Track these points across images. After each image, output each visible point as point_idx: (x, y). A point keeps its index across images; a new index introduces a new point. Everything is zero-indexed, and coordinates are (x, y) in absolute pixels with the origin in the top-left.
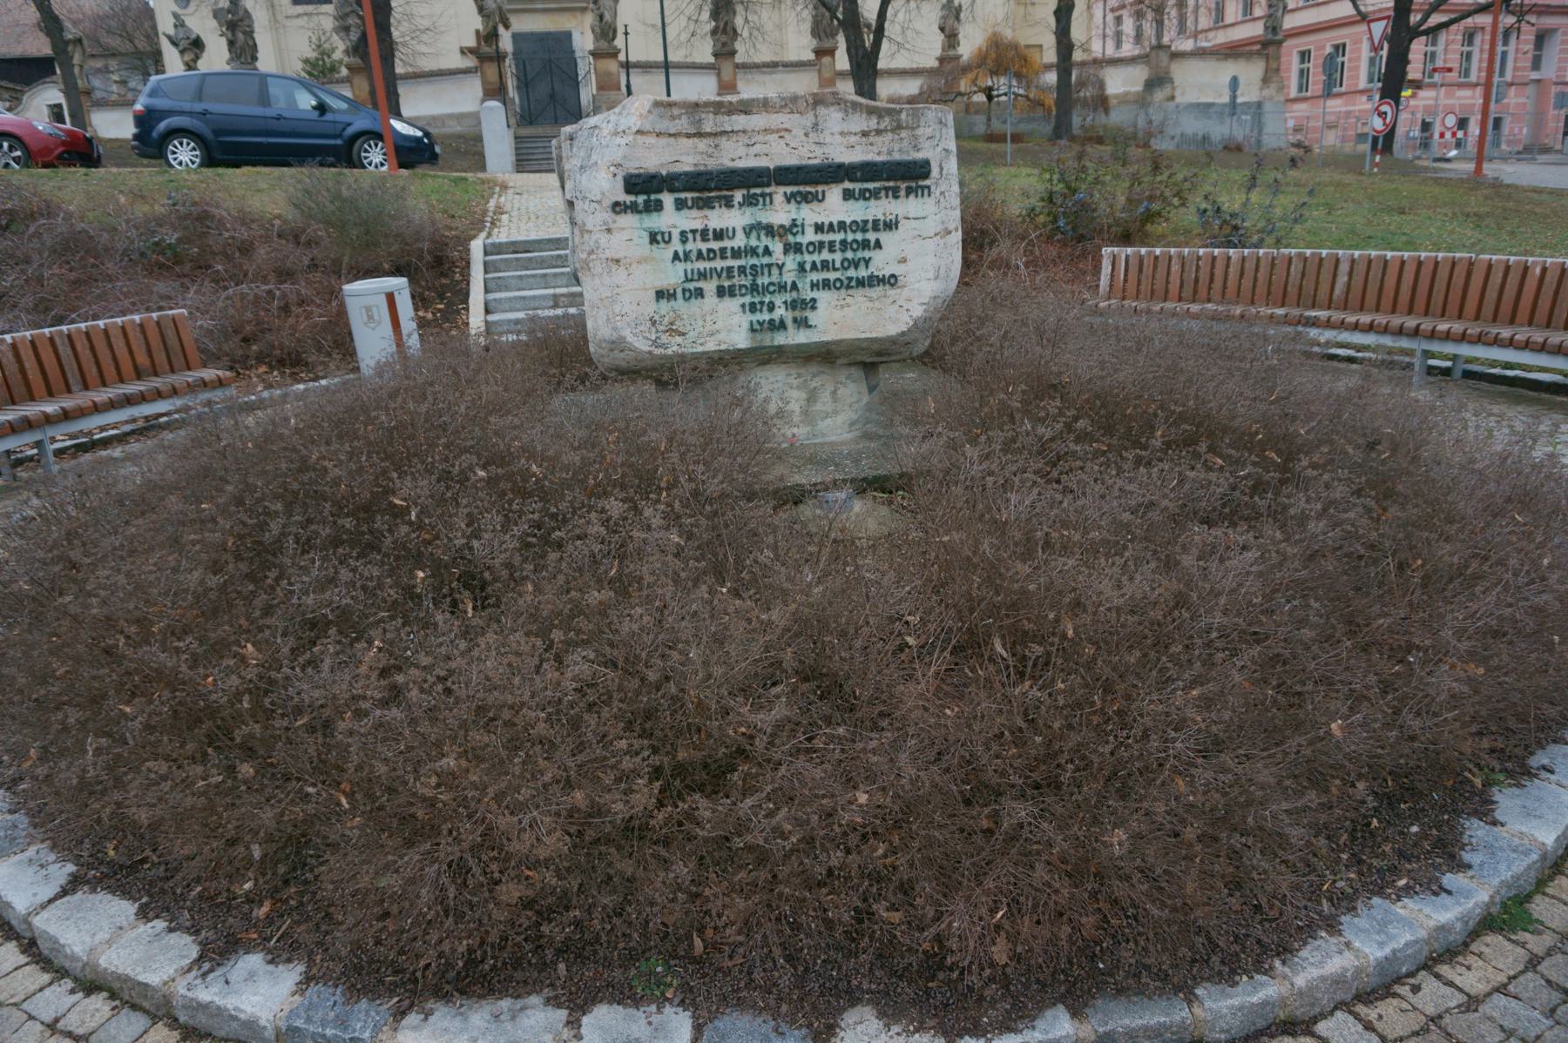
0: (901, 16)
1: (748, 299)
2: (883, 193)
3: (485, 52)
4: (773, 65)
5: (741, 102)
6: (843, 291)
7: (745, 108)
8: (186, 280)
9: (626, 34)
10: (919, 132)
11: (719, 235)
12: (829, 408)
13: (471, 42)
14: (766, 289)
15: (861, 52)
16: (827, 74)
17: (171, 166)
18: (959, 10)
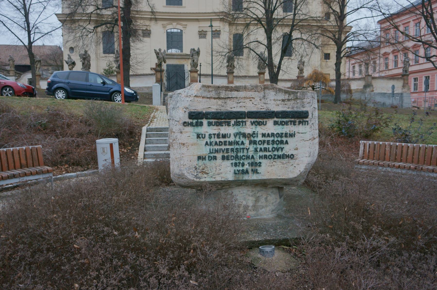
0: (286, 64)
1: (234, 161)
2: (289, 123)
3: (158, 69)
4: (245, 77)
5: (236, 87)
6: (272, 160)
7: (237, 89)
8: (46, 135)
9: (200, 66)
11: (224, 136)
12: (264, 204)
13: (154, 66)
14: (241, 158)
15: (273, 74)
16: (262, 80)
17: (56, 98)
18: (304, 62)
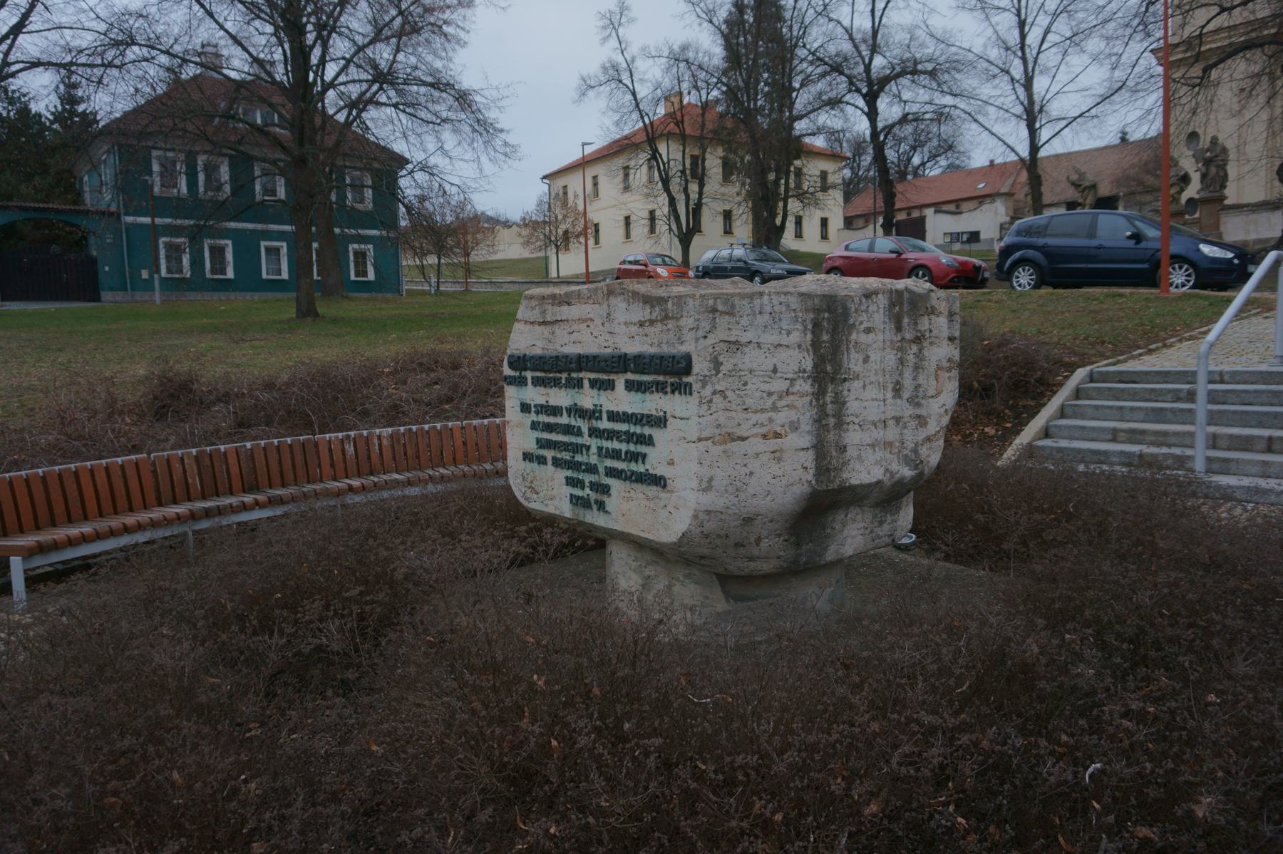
10: (683, 322)
17: (1013, 287)
